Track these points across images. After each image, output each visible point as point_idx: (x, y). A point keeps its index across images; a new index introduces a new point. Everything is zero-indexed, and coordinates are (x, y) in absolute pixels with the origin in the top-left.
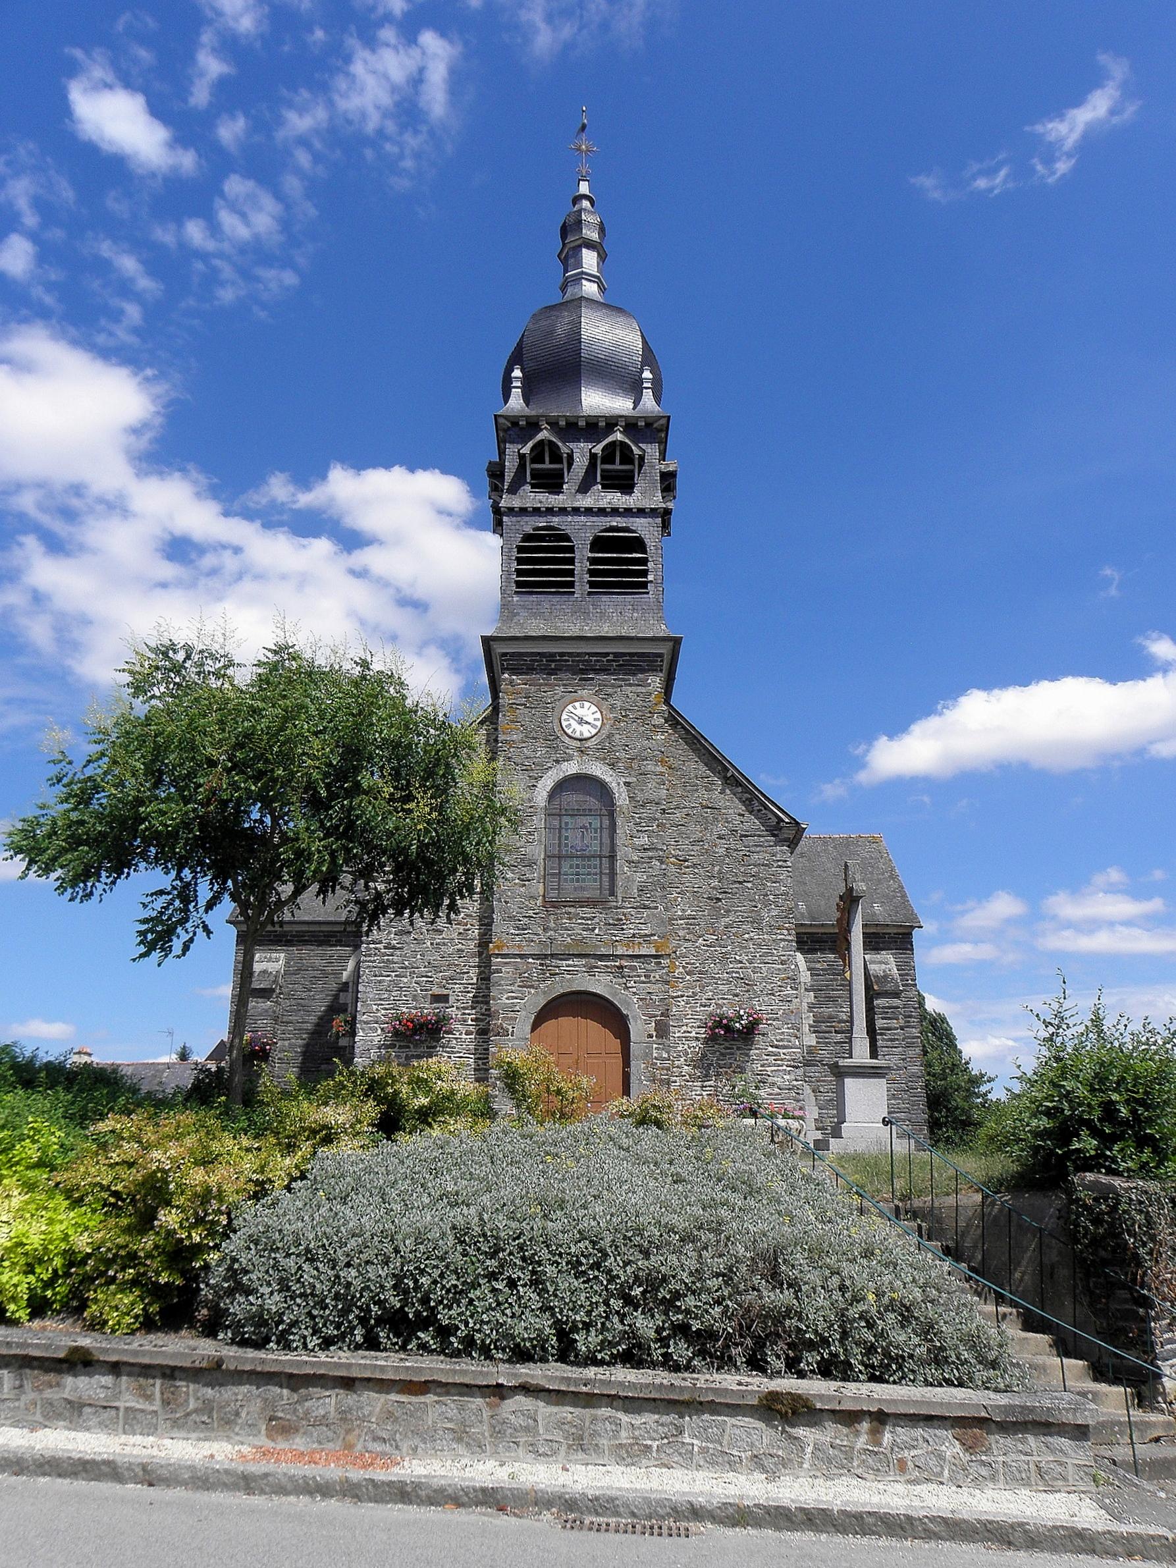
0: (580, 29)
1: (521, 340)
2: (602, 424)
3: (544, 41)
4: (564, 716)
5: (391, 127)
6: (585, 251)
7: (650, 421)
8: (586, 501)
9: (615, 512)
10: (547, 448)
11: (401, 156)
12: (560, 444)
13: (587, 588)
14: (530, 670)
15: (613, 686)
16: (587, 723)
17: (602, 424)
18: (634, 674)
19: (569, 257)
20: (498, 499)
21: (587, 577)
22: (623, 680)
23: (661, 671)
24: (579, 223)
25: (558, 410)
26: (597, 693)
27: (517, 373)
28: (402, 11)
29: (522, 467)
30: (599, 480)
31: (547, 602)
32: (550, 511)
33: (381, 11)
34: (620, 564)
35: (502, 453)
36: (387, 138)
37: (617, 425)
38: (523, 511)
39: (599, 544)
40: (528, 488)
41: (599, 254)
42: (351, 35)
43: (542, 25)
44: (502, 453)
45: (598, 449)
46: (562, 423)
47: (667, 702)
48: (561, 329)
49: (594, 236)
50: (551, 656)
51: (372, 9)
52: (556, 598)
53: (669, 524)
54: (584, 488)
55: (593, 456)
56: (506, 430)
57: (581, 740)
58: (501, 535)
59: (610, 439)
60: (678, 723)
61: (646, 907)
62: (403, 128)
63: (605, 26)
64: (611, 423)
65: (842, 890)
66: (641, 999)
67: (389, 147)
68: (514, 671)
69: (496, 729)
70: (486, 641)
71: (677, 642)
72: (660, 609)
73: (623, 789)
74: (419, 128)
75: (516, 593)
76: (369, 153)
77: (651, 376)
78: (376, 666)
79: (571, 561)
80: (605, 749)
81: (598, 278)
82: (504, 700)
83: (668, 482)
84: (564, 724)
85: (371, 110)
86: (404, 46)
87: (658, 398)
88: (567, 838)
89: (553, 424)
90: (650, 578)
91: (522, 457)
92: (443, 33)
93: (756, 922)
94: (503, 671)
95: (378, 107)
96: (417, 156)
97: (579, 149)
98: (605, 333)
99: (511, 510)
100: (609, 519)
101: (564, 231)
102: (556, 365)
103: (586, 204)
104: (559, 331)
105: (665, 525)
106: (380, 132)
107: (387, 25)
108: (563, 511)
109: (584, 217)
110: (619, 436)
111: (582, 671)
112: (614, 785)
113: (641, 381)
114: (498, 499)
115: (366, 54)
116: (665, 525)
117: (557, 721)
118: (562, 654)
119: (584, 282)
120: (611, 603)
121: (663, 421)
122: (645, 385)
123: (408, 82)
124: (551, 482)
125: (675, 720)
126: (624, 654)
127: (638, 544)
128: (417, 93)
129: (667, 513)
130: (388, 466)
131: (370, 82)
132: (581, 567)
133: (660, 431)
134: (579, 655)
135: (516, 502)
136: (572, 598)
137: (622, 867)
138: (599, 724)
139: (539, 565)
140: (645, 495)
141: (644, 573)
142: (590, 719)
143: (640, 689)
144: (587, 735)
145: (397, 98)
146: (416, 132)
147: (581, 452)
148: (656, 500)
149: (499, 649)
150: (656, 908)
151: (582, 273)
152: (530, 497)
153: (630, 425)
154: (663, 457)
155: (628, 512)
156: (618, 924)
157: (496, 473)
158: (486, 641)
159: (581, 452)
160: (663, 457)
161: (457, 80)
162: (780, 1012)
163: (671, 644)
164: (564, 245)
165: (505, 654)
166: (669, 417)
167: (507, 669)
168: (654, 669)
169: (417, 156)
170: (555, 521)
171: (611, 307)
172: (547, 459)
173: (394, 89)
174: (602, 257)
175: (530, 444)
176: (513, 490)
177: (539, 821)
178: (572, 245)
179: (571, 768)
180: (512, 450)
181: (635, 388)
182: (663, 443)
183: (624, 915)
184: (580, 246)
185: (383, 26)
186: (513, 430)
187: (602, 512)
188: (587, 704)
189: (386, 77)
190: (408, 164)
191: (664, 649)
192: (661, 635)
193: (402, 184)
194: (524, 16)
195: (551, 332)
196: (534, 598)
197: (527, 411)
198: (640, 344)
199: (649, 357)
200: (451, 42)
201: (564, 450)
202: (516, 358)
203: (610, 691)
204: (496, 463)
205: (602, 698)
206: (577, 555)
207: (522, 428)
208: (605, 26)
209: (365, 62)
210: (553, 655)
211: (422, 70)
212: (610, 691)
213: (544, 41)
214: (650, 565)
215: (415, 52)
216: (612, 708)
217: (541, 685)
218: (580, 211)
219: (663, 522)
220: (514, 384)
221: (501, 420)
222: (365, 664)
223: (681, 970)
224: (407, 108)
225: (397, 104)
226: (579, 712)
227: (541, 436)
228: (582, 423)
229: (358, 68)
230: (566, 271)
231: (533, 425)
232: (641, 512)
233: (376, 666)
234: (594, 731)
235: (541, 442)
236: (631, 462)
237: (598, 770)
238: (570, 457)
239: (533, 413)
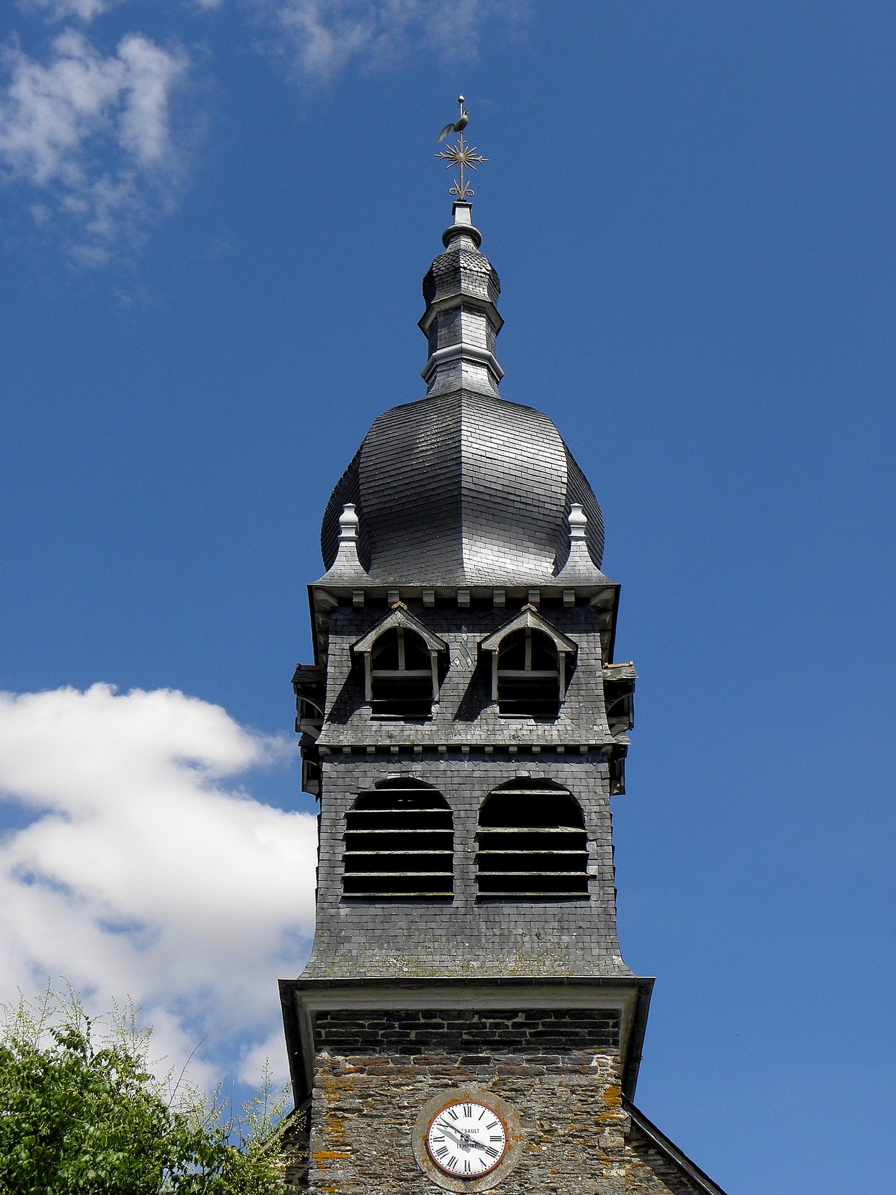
0: (377, 33)
1: (359, 454)
2: (500, 600)
3: (320, 50)
4: (435, 1132)
5: (73, 173)
6: (465, 318)
7: (584, 594)
8: (473, 734)
9: (525, 752)
10: (401, 643)
11: (92, 216)
12: (425, 635)
13: (475, 890)
14: (369, 1044)
15: (525, 1073)
16: (477, 1145)
17: (500, 600)
18: (566, 1051)
19: (438, 324)
20: (311, 731)
21: (474, 870)
22: (546, 1062)
23: (616, 1043)
24: (455, 273)
25: (422, 576)
26: (495, 1088)
27: (349, 515)
28: (94, 12)
29: (355, 678)
30: (495, 695)
31: (402, 916)
32: (407, 752)
33: (60, 12)
34: (536, 845)
35: (321, 650)
36: (69, 191)
37: (525, 601)
38: (359, 753)
39: (494, 809)
40: (367, 711)
41: (490, 322)
42: (12, 45)
43: (316, 30)
44: (321, 650)
45: (493, 643)
46: (429, 599)
47: (627, 1103)
48: (427, 439)
49: (482, 292)
50: (408, 1018)
51: (47, 12)
52: (417, 910)
53: (622, 773)
54: (468, 711)
55: (484, 657)
56: (328, 613)
57: (465, 1179)
58: (319, 796)
59: (515, 625)
60: (651, 1144)
62: (93, 175)
63: (415, 31)
64: (516, 598)
67: (70, 203)
68: (341, 1046)
69: (305, 1160)
70: (289, 989)
71: (643, 988)
72: (611, 927)
74: (120, 175)
75: (345, 900)
76: (39, 212)
77: (584, 519)
78: (97, 1044)
79: (447, 841)
81: (489, 359)
82: (322, 1101)
83: (619, 699)
84: (435, 1147)
85: (42, 149)
86: (97, 58)
87: (596, 557)
89: (413, 602)
90: (592, 870)
91: (357, 658)
92: (158, 39)
94: (320, 1045)
95: (53, 145)
96: (117, 215)
97: (454, 159)
98: (506, 448)
99: (336, 752)
100: (513, 765)
101: (430, 285)
102: (415, 501)
103: (465, 242)
104: (423, 446)
105: (616, 777)
106: (57, 182)
107: (68, 30)
108: (431, 752)
109: (463, 263)
110: (529, 620)
111: (468, 1046)
113: (567, 527)
114: (311, 731)
115: (37, 71)
116: (616, 777)
117: (419, 1142)
118: (429, 1014)
119: (465, 366)
120: (515, 916)
121: (608, 595)
122: (574, 533)
123: (102, 111)
124: (409, 701)
125: (644, 1138)
126: (545, 1013)
127: (569, 809)
128: (117, 126)
129: (617, 754)
130: (82, 686)
131: (42, 109)
132: (464, 851)
133: (602, 610)
134: (460, 1014)
135: (345, 737)
136: (448, 909)
138: (499, 1146)
139: (386, 851)
140: (579, 721)
141: (581, 862)
142: (483, 1137)
143: (576, 1079)
144: (477, 1168)
145: (84, 132)
146: (116, 182)
147: (463, 649)
148: (599, 731)
149: (312, 1004)
151: (462, 351)
152: (369, 728)
153: (551, 602)
154: (609, 655)
155: (549, 753)
157: (310, 685)
158: (289, 989)
159: (463, 649)
160: (609, 655)
161: (179, 108)
163: (632, 993)
164: (430, 307)
165: (322, 1015)
166: (617, 588)
167: (327, 1042)
168: (602, 1041)
169: (117, 215)
170: (417, 769)
171: (513, 402)
172: (402, 662)
173: (79, 120)
174: (495, 325)
175: (372, 636)
176: (341, 716)
178: (444, 307)
180: (339, 647)
181: (557, 539)
182: (609, 633)
184: (457, 309)
185: (62, 31)
186: (338, 611)
187: (501, 753)
188: (477, 1110)
189: (68, 103)
190: (102, 226)
191: (621, 1002)
192: (614, 975)
193: (94, 257)
194: (287, 17)
195: (409, 448)
196: (376, 909)
197: (367, 580)
198: (562, 466)
199: (579, 486)
200: (171, 53)
201: (433, 645)
202: (348, 490)
203: (521, 1083)
204: (309, 669)
205: (505, 1096)
206: (458, 831)
207: (357, 609)
208: (415, 31)
209: (35, 81)
210: (411, 1015)
211: (124, 93)
212: (521, 1083)
213: (320, 50)
214: (591, 847)
215: (114, 68)
216: (525, 1116)
217: (390, 1072)
218: (457, 253)
219: (612, 770)
220: (344, 534)
221: (321, 596)
222: (74, 1042)
224: (101, 145)
225: (85, 142)
226: (463, 1123)
227: (390, 622)
228: (464, 599)
229: (22, 89)
230: (433, 348)
231: (376, 604)
232: (572, 753)
233: (97, 1044)
234: (490, 1161)
235: (392, 633)
236: (554, 666)
238: (444, 658)
239: (378, 583)
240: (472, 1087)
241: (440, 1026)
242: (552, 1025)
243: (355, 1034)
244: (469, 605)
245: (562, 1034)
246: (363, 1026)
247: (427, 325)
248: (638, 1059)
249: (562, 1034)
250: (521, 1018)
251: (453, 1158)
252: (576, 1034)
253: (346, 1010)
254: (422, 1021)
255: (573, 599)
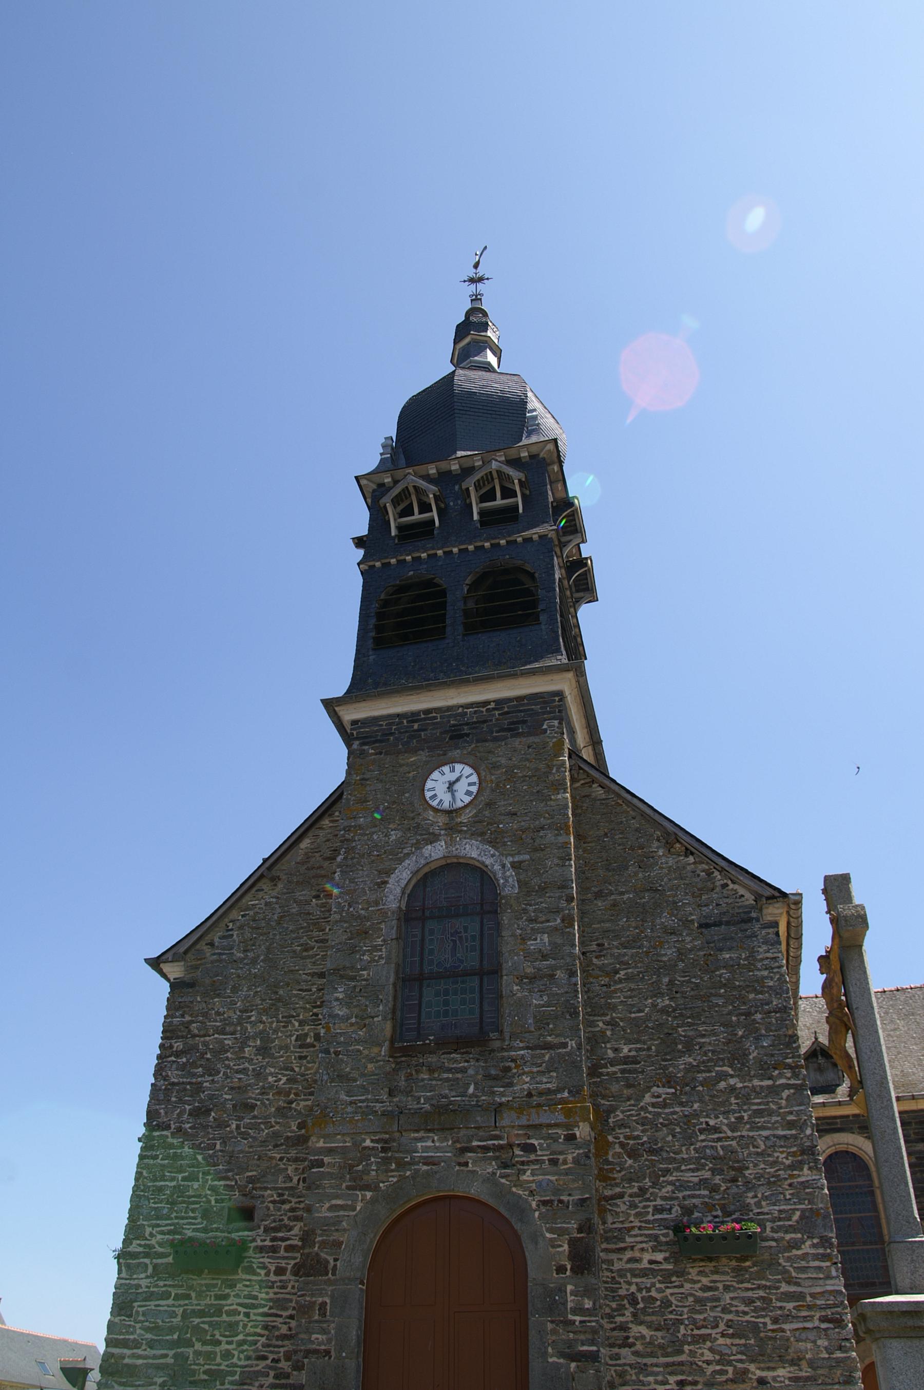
61: (548, 1047)
65: (433, 364)
66: (545, 1203)
73: (510, 872)
80: (481, 820)
88: (431, 952)
93: (738, 1058)
112: (497, 867)
126: (509, 700)
134: (449, 708)
137: (512, 988)
150: (565, 1045)
156: (504, 1077)
162: (796, 1217)
165: (354, 722)
177: (389, 929)
179: (436, 851)
183: (514, 1060)
221: (363, 482)
223: (618, 1149)
237: (472, 850)
240: (456, 753)
241: (435, 718)
242: (516, 706)
243: (377, 731)
244: (459, 472)
245: (521, 711)
246: (382, 725)
247: (455, 361)
248: (600, 742)
249: (521, 711)
250: (492, 705)
251: (441, 800)
252: (532, 710)
253: (370, 717)
254: (423, 716)
255: (526, 454)
